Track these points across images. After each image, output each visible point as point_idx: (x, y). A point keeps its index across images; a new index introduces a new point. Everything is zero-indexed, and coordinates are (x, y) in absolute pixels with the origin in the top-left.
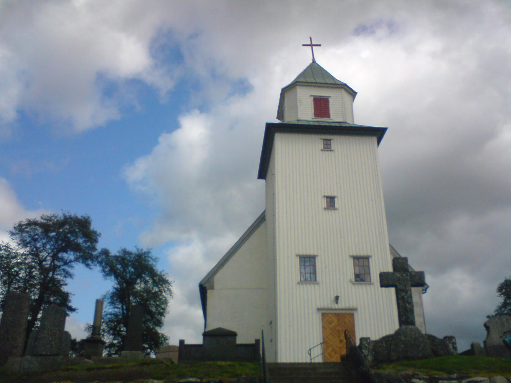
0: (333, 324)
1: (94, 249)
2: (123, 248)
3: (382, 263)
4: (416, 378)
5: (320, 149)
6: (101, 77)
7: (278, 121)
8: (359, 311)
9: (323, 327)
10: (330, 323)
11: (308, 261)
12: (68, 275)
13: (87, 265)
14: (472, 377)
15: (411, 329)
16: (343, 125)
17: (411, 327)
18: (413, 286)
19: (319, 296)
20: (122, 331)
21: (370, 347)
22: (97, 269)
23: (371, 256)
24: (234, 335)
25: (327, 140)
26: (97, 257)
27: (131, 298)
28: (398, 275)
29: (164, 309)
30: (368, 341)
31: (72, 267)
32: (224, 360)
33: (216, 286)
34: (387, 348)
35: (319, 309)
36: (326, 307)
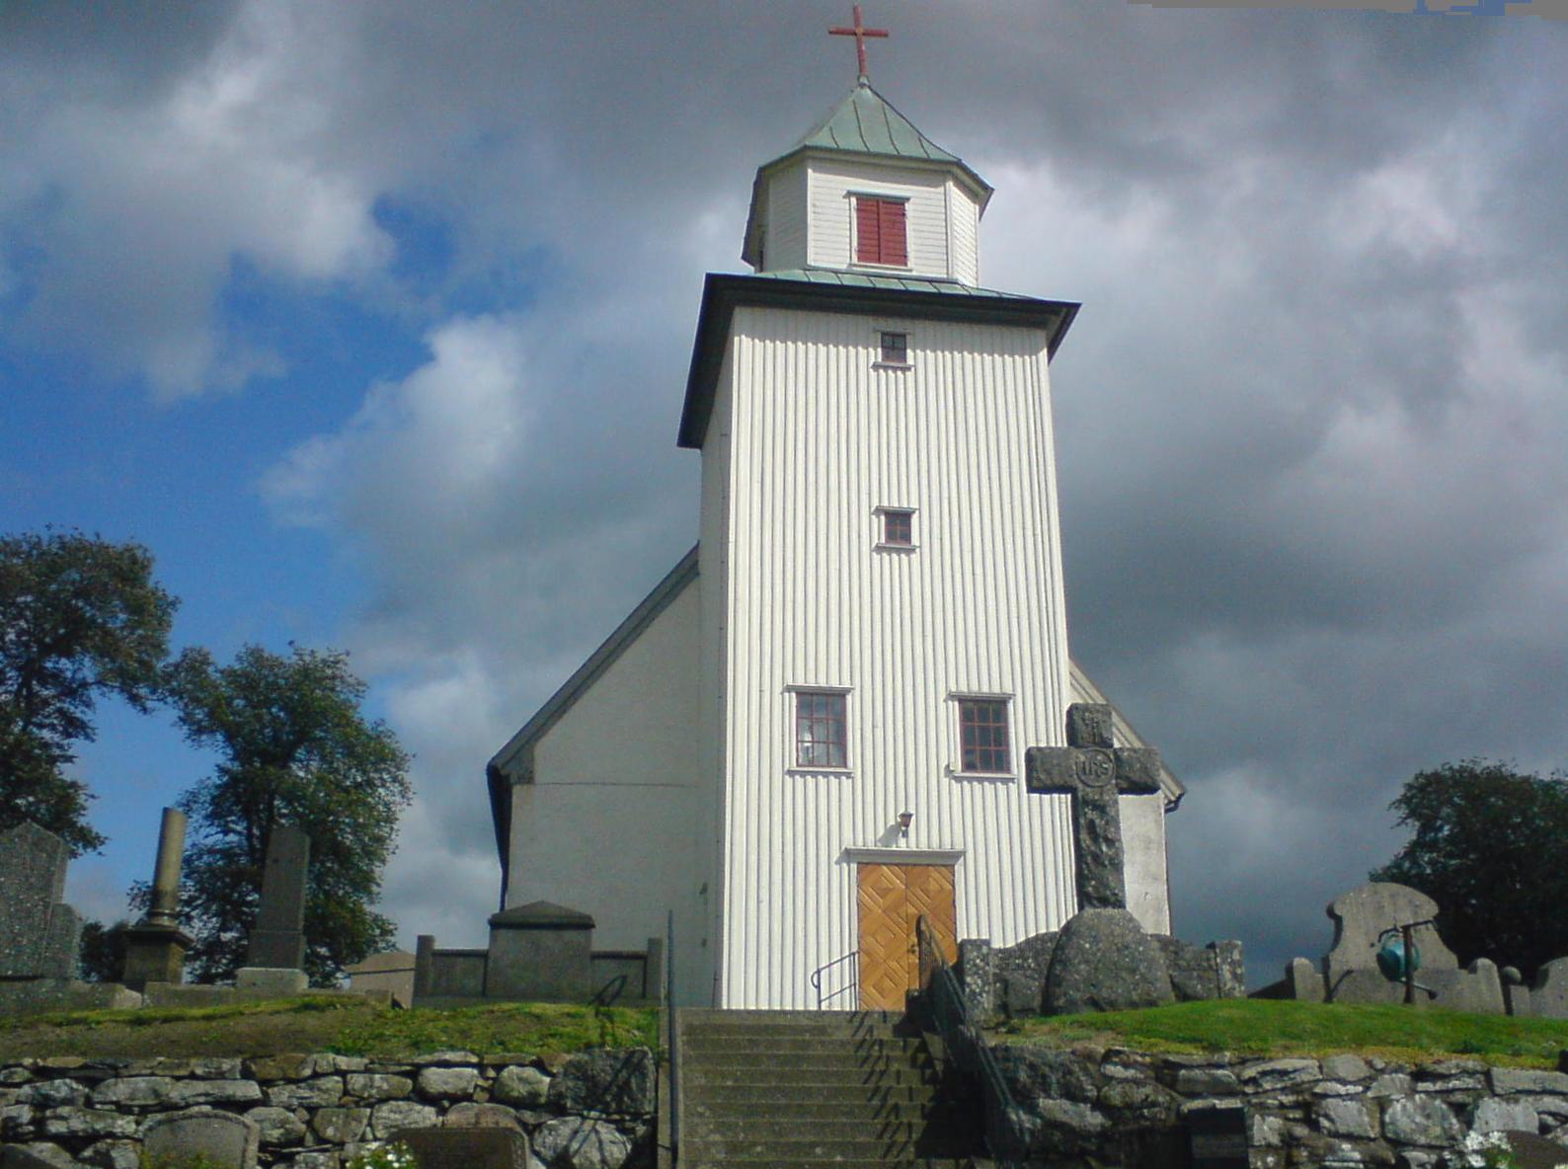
0: (891, 897)
1: (159, 648)
2: (252, 645)
3: (1035, 726)
4: (1116, 1064)
6: (241, 266)
7: (747, 270)
10: (884, 893)
11: (822, 711)
12: (74, 727)
13: (134, 699)
14: (1271, 1059)
15: (1111, 918)
16: (945, 289)
17: (1110, 911)
18: (1122, 791)
19: (851, 810)
20: (250, 904)
21: (991, 970)
22: (167, 713)
24: (585, 924)
25: (894, 335)
26: (168, 677)
27: (276, 802)
28: (1082, 758)
29: (380, 840)
30: (985, 950)
32: (553, 997)
33: (542, 772)
34: (1050, 972)
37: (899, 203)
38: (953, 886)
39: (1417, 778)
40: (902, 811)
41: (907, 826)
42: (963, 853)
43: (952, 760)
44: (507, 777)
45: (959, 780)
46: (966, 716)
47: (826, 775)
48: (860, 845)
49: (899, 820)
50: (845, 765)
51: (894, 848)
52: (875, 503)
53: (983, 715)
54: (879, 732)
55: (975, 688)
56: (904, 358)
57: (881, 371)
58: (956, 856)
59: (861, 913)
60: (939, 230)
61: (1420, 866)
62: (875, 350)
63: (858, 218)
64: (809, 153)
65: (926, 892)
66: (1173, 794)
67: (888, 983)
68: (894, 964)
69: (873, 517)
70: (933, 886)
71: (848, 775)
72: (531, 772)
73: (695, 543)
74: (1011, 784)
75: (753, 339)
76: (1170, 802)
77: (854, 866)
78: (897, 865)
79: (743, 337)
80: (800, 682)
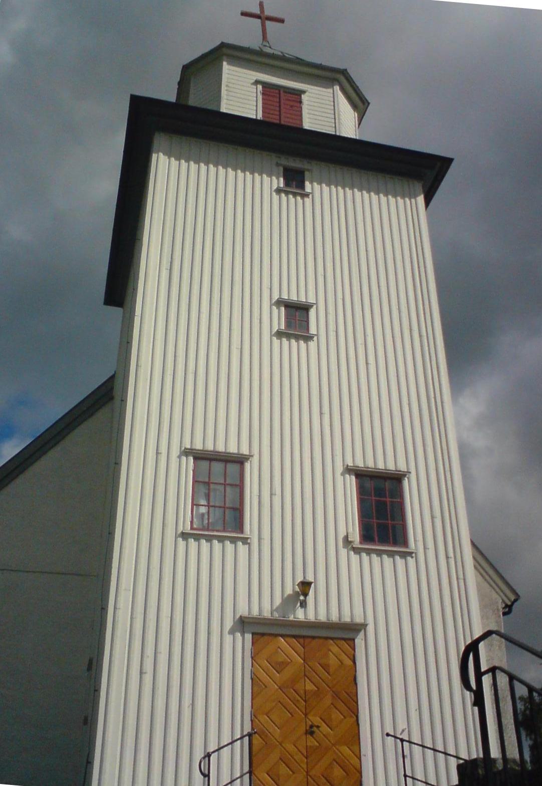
0: (288, 673)
5: (275, 187)
10: (280, 667)
11: (220, 480)
19: (249, 578)
31: (260, 48)
37: (299, 93)
38: (354, 663)
40: (300, 579)
41: (306, 595)
42: (364, 626)
43: (351, 530)
45: (357, 551)
47: (221, 539)
48: (255, 612)
49: (297, 589)
50: (241, 530)
51: (291, 618)
52: (276, 297)
53: (379, 492)
54: (277, 500)
55: (371, 464)
56: (302, 187)
57: (283, 195)
58: (355, 628)
59: (255, 689)
60: (330, 107)
62: (278, 178)
63: (263, 99)
64: (225, 50)
65: (326, 667)
66: (509, 599)
67: (283, 770)
68: (291, 748)
69: (274, 308)
70: (332, 661)
71: (245, 541)
73: (114, 373)
74: (409, 558)
75: (169, 158)
76: (507, 606)
77: (248, 637)
78: (294, 637)
79: (161, 154)
80: (199, 446)
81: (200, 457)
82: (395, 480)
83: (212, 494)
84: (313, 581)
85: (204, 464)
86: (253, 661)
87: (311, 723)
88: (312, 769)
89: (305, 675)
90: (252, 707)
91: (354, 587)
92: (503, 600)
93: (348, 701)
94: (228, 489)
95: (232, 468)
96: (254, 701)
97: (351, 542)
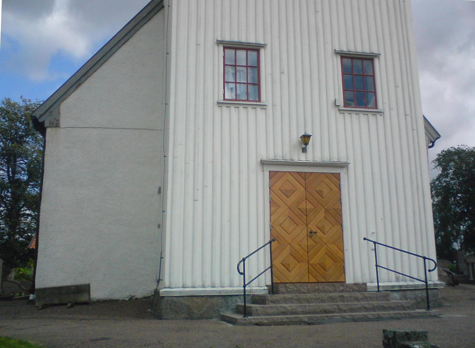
0: (293, 198)
2: (7, 98)
8: (351, 166)
9: (272, 203)
19: (264, 135)
23: (377, 56)
35: (263, 163)
36: (280, 158)
39: (442, 152)
44: (43, 123)
46: (345, 71)
61: (441, 183)
72: (58, 120)
81: (227, 46)
82: (369, 59)
83: (238, 74)
84: (311, 135)
85: (230, 53)
86: (271, 191)
87: (310, 230)
88: (311, 260)
89: (306, 199)
90: (270, 222)
91: (342, 137)
92: (429, 139)
93: (336, 216)
94: (249, 68)
95: (253, 55)
96: (271, 217)
97: (338, 106)
